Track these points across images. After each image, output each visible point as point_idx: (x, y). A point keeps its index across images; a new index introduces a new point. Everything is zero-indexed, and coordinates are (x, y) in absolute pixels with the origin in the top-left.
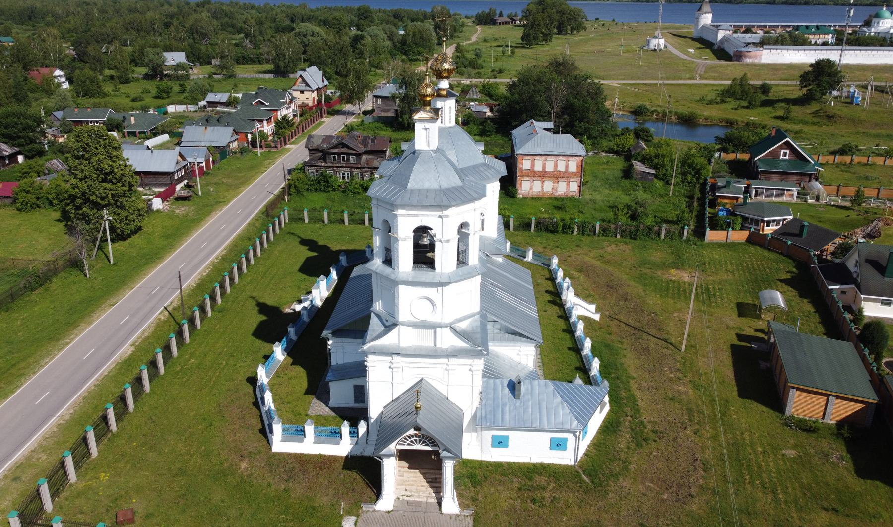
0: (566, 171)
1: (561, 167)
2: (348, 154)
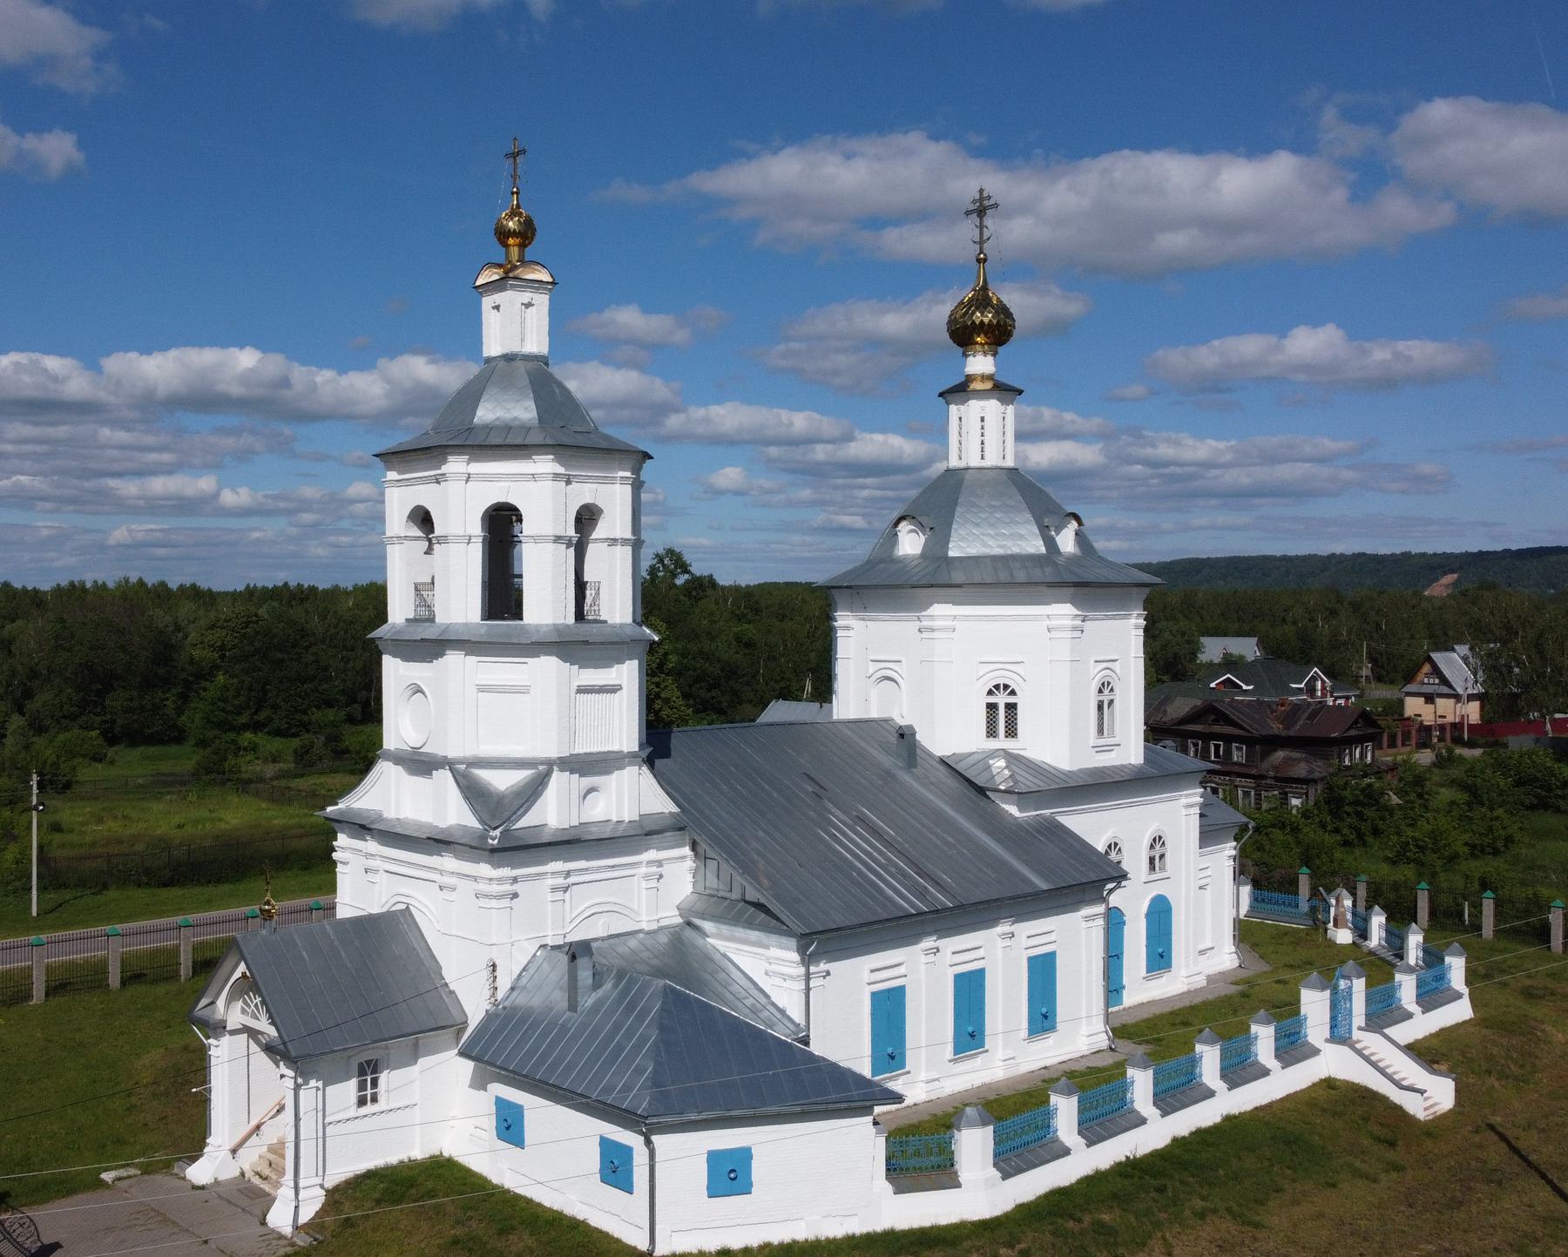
2: (1228, 739)
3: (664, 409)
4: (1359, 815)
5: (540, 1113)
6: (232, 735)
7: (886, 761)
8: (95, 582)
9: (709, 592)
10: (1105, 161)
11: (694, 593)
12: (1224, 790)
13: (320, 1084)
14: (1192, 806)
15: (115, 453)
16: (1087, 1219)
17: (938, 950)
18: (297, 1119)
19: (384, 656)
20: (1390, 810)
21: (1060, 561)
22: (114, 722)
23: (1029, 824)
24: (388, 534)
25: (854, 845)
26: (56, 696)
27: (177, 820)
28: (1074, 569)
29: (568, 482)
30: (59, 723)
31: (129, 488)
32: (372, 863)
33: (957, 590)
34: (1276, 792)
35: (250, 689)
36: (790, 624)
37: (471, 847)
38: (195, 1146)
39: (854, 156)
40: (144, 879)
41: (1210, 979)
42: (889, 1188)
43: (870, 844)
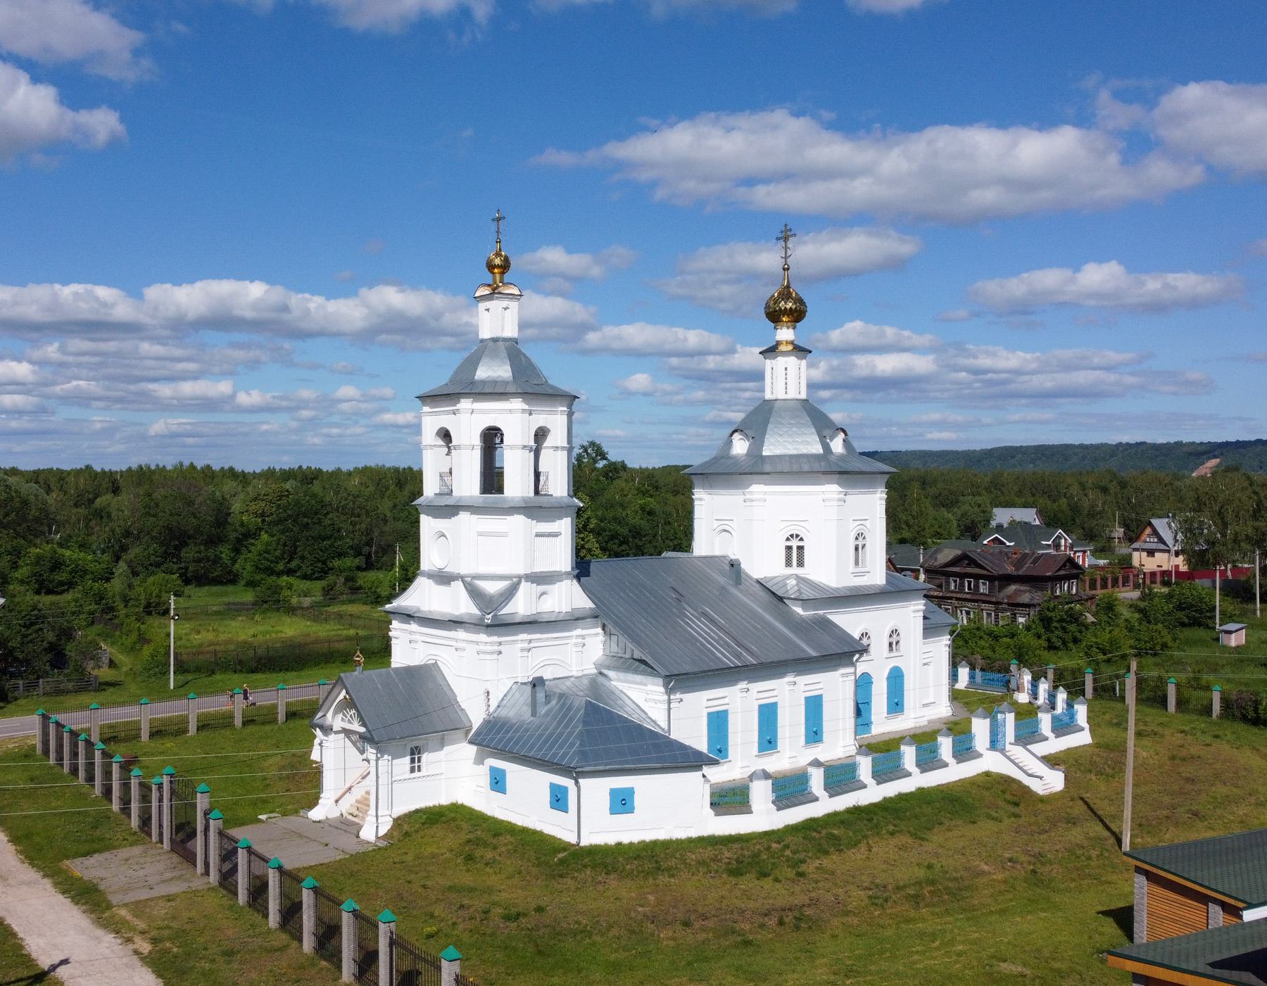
3: (584, 328)
4: (1064, 628)
5: (515, 773)
6: (274, 578)
7: (722, 580)
8: (157, 465)
9: (622, 473)
10: (931, 133)
11: (610, 474)
12: (974, 612)
13: (390, 758)
14: (918, 611)
15: (152, 363)
16: (824, 832)
17: (748, 690)
18: (377, 777)
19: (421, 515)
20: (1087, 627)
21: (832, 458)
22: (187, 568)
23: (811, 620)
24: (424, 443)
25: (698, 628)
26: (145, 549)
27: (251, 632)
28: (840, 463)
29: (530, 414)
30: (147, 569)
31: (164, 391)
32: (413, 637)
33: (766, 476)
34: (1009, 614)
35: (285, 545)
36: (682, 497)
37: (475, 625)
38: (313, 802)
39: (733, 129)
40: (239, 667)
41: (929, 722)
42: (712, 812)
43: (709, 629)
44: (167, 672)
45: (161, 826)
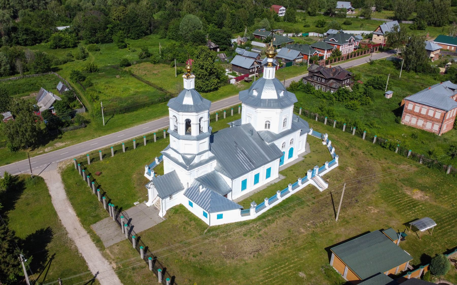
0: (433, 117)
1: (431, 113)
2: (322, 78)
38: (147, 199)
44: (101, 116)
45: (112, 213)
